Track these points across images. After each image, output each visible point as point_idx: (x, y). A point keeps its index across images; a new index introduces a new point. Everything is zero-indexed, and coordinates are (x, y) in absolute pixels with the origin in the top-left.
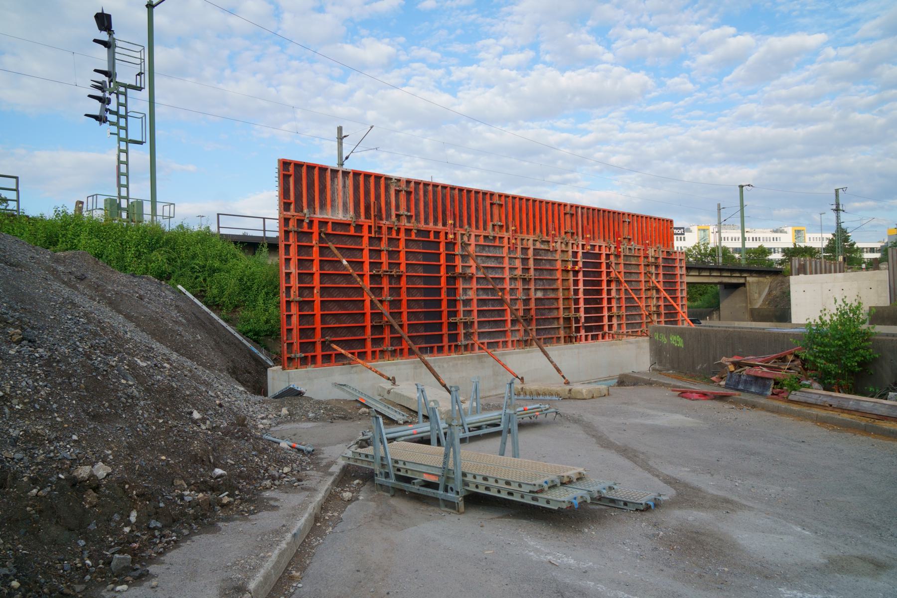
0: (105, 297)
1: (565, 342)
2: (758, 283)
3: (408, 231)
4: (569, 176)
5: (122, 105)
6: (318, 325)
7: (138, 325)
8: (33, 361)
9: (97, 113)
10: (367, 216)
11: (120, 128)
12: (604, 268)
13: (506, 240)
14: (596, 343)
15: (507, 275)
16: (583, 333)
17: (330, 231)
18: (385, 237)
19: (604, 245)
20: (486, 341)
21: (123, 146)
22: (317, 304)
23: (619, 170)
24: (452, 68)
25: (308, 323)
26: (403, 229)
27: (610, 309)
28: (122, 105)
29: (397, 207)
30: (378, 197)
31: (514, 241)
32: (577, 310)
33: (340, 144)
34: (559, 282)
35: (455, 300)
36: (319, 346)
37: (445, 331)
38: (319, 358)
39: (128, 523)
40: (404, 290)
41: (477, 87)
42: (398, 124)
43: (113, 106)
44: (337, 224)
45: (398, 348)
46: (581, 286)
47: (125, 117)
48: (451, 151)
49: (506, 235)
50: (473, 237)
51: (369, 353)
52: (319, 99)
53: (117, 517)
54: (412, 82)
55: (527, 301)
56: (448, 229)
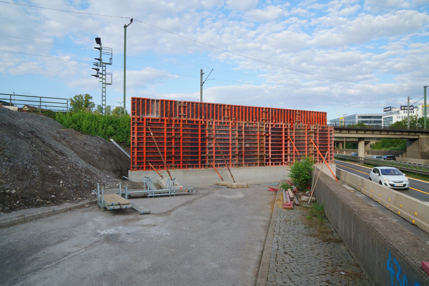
0: (70, 145)
1: (260, 165)
2: (427, 138)
3: (184, 121)
4: (368, 76)
5: (104, 71)
6: (145, 156)
7: (78, 154)
8: (8, 166)
9: (96, 74)
10: (166, 116)
11: (103, 79)
12: (283, 135)
13: (230, 124)
14: (277, 166)
15: (230, 137)
16: (270, 162)
17: (150, 122)
18: (173, 123)
19: (284, 125)
20: (219, 164)
21: (104, 85)
22: (145, 148)
23: (398, 72)
24: (312, 19)
25: (141, 155)
26: (181, 120)
27: (286, 152)
28: (104, 71)
29: (180, 112)
30: (171, 109)
31: (234, 124)
32: (268, 152)
33: (202, 77)
34: (258, 140)
35: (206, 148)
36: (145, 163)
37: (200, 159)
38: (145, 168)
39: (16, 203)
40: (181, 143)
41: (324, 29)
42: (278, 51)
43: (101, 71)
44: (153, 119)
45: (178, 165)
46: (270, 142)
47: (105, 75)
48: (304, 64)
49: (231, 122)
50: (214, 123)
51: (200, 166)
52: (240, 40)
53: (13, 201)
54: (290, 28)
55: (240, 148)
56: (202, 120)
